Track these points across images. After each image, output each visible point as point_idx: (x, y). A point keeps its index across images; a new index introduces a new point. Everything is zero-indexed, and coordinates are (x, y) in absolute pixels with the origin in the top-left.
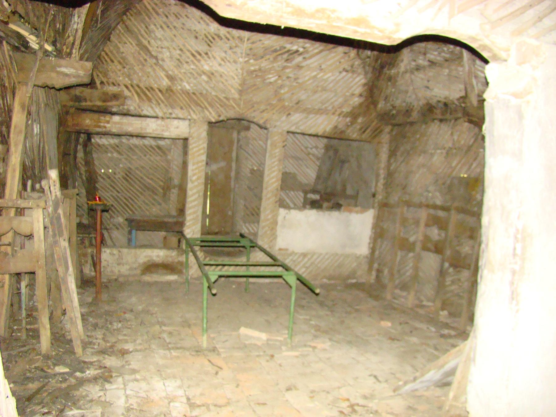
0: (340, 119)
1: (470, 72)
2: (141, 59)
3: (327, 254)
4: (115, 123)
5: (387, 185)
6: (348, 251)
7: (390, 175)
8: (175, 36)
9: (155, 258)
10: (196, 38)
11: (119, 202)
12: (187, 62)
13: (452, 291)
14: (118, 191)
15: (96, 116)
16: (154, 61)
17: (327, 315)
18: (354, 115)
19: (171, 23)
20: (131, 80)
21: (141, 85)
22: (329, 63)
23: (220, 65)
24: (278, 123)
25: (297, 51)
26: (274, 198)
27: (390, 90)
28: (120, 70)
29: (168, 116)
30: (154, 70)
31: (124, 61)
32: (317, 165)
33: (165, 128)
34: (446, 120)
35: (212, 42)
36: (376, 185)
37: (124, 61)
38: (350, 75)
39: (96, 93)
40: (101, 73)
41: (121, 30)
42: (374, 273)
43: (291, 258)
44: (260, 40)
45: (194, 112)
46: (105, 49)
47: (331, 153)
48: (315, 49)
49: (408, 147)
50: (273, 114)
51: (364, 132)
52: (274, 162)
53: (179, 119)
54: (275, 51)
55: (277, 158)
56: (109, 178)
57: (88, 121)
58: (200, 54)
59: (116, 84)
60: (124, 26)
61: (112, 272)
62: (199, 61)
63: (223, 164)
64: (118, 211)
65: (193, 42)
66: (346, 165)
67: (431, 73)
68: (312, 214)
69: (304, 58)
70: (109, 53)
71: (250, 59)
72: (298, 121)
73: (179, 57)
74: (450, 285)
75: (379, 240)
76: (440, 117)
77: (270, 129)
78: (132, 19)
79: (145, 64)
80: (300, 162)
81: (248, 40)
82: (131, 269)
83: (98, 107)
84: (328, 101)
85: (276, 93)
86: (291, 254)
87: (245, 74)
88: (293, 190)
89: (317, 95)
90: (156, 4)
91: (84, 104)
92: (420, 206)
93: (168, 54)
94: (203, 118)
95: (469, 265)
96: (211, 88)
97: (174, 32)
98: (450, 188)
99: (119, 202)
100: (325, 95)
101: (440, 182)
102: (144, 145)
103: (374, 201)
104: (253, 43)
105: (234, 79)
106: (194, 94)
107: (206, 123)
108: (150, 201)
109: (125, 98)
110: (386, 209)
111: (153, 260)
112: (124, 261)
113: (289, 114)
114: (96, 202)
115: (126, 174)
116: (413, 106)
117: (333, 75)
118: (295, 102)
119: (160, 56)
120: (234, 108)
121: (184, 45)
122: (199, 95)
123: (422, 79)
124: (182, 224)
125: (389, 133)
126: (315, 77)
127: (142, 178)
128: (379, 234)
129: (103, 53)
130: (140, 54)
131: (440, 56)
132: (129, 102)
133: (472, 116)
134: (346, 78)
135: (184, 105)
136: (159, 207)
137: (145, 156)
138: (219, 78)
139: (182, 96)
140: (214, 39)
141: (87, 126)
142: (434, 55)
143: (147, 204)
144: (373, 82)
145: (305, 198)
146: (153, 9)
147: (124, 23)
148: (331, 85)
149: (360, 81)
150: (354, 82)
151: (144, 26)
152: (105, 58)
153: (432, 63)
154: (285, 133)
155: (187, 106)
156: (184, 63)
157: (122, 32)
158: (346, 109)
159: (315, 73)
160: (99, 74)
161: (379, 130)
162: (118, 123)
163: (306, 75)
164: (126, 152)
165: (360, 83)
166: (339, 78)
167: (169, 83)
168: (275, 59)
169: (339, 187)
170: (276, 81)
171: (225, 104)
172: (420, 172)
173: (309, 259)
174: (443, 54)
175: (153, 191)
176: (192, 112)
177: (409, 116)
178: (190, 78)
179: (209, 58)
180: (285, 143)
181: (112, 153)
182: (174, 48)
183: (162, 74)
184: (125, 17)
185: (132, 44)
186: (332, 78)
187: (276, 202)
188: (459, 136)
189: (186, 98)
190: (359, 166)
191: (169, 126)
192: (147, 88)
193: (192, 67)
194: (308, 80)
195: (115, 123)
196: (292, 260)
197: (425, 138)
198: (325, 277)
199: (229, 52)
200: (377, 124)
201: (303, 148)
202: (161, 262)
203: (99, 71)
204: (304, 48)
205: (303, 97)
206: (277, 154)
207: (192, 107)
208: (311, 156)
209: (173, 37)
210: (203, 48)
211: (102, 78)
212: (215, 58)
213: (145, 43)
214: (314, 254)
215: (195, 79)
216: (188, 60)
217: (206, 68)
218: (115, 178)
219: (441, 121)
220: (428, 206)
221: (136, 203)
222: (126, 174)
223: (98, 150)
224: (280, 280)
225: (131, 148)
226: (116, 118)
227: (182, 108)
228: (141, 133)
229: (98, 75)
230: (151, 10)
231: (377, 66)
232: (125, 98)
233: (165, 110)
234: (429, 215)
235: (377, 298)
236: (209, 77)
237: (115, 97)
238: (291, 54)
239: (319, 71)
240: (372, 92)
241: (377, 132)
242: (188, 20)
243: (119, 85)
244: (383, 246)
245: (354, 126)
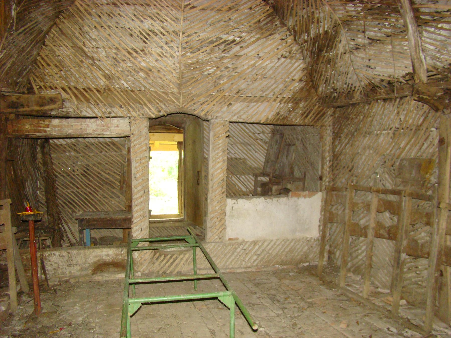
0: (282, 106)
1: (417, 45)
2: (77, 60)
3: (277, 240)
5: (332, 168)
6: (299, 235)
7: (335, 157)
8: (109, 35)
9: (104, 257)
10: (131, 35)
11: (79, 198)
12: (124, 61)
13: (410, 279)
14: (78, 188)
15: (35, 121)
16: (91, 62)
17: (278, 316)
18: (295, 100)
19: (105, 22)
20: (68, 82)
21: (79, 87)
22: (266, 51)
23: (157, 60)
24: (219, 115)
25: (234, 41)
27: (330, 72)
28: (57, 74)
29: (108, 115)
30: (91, 71)
31: (60, 64)
32: (265, 149)
33: (105, 128)
34: (391, 99)
35: (147, 39)
36: (323, 168)
37: (60, 64)
38: (289, 60)
39: (33, 98)
40: (37, 77)
41: (55, 33)
42: (326, 255)
44: (196, 33)
45: (133, 109)
46: (41, 54)
47: (277, 137)
48: (251, 37)
49: (352, 129)
50: (214, 105)
51: (307, 116)
52: (218, 153)
53: (120, 117)
54: (212, 42)
55: (221, 149)
56: (69, 175)
57: (27, 127)
58: (136, 52)
59: (53, 87)
60: (57, 29)
61: (63, 273)
62: (135, 58)
64: (79, 206)
65: (127, 39)
66: (293, 148)
67: (372, 51)
68: (260, 203)
69: (241, 47)
70: (46, 58)
71: (187, 52)
72: (239, 110)
73: (115, 56)
74: (407, 272)
75: (329, 225)
76: (384, 96)
77: (212, 121)
78: (65, 21)
79: (82, 65)
80: (249, 147)
81: (183, 33)
82: (82, 270)
83: (37, 111)
84: (269, 88)
85: (216, 84)
86: (241, 244)
87: (183, 68)
88: (244, 174)
89: (257, 84)
90: (88, 5)
91: (21, 110)
92: (370, 190)
93: (104, 54)
94: (143, 115)
95: (429, 254)
96: (149, 84)
97: (108, 31)
98: (400, 171)
99: (79, 198)
100: (265, 83)
101: (389, 164)
102: (100, 143)
103: (321, 184)
104: (189, 36)
105: (172, 73)
106: (132, 91)
107: (147, 120)
108: (108, 195)
109: (63, 101)
110: (334, 193)
111: (104, 259)
112: (74, 262)
113: (230, 104)
114: (27, 213)
115: (84, 171)
116: (355, 87)
117: (271, 62)
118: (235, 92)
119: (96, 56)
120: (174, 102)
121: (120, 44)
122: (137, 92)
123: (363, 58)
124: (129, 221)
125: (331, 115)
126: (254, 65)
127: (99, 173)
128: (328, 218)
129: (39, 58)
130: (76, 56)
131: (380, 32)
132: (67, 104)
133: (423, 93)
134: (286, 63)
135: (123, 104)
136: (117, 199)
137: (101, 152)
138: (156, 74)
139: (120, 94)
140: (148, 35)
141: (26, 131)
142: (375, 32)
143: (105, 197)
144: (312, 66)
145: (256, 181)
146: (85, 10)
147: (57, 26)
148: (271, 72)
149: (299, 66)
150: (293, 68)
151: (78, 28)
152: (40, 62)
153: (372, 41)
154: (227, 123)
155: (126, 104)
156: (121, 61)
157: (57, 35)
158: (287, 95)
159: (253, 62)
160: (36, 79)
161: (322, 113)
162: (58, 126)
163: (244, 65)
164: (83, 150)
165: (299, 68)
166: (278, 64)
167: (107, 83)
168: (212, 50)
169: (287, 170)
170: (214, 72)
171: (164, 99)
172: (366, 154)
173: (260, 247)
174: (384, 30)
175: (111, 184)
176: (131, 110)
177: (352, 97)
178: (127, 76)
179: (145, 54)
180: (228, 133)
181: (70, 151)
182: (109, 47)
183: (99, 74)
184: (58, 20)
185: (67, 47)
186: (272, 65)
187: (223, 193)
188: (406, 116)
189: (124, 96)
190: (305, 149)
191: (109, 125)
192: (84, 89)
193: (129, 64)
194: (248, 68)
195: (55, 127)
196: (242, 249)
197: (369, 119)
198: (277, 263)
199: (166, 47)
200: (319, 107)
201: (250, 134)
202: (111, 260)
203: (36, 75)
204: (240, 37)
205: (243, 86)
206: (221, 145)
207: (131, 104)
208: (258, 141)
209: (108, 36)
210: (139, 45)
211: (39, 82)
212: (151, 54)
213: (81, 44)
214: (265, 241)
215: (132, 76)
216: (125, 58)
217: (143, 64)
218: (74, 175)
219: (385, 100)
220: (378, 191)
221: (95, 197)
222: (84, 171)
223: (56, 150)
224: (216, 301)
225: (87, 146)
226: (56, 122)
227: (121, 107)
228: (81, 134)
229: (35, 80)
230: (84, 12)
231: (315, 49)
232: (63, 101)
233: (104, 110)
234: (380, 200)
235: (330, 285)
236: (147, 74)
237: (52, 100)
238: (228, 44)
239: (257, 59)
240: (312, 77)
241: (320, 115)
242: (122, 18)
243: (56, 88)
244: (334, 228)
245: (297, 111)
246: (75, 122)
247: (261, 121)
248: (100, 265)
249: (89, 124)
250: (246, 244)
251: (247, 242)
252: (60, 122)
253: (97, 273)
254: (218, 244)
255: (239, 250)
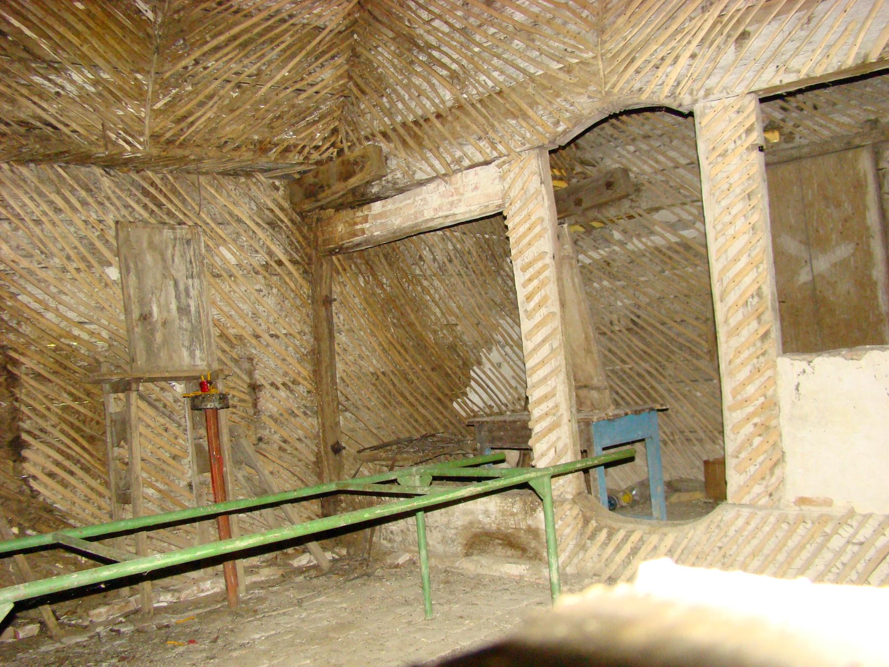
4: (377, 217)
9: (481, 517)
26: (754, 324)
43: (846, 532)
63: (844, 251)
86: (842, 522)
127: (663, 324)
202: (494, 527)
246: (405, 200)
247: (866, 56)
248: (476, 536)
249: (427, 196)
250: (862, 524)
251: (867, 517)
252: (383, 206)
253: (472, 554)
254: (760, 514)
255: (836, 542)
